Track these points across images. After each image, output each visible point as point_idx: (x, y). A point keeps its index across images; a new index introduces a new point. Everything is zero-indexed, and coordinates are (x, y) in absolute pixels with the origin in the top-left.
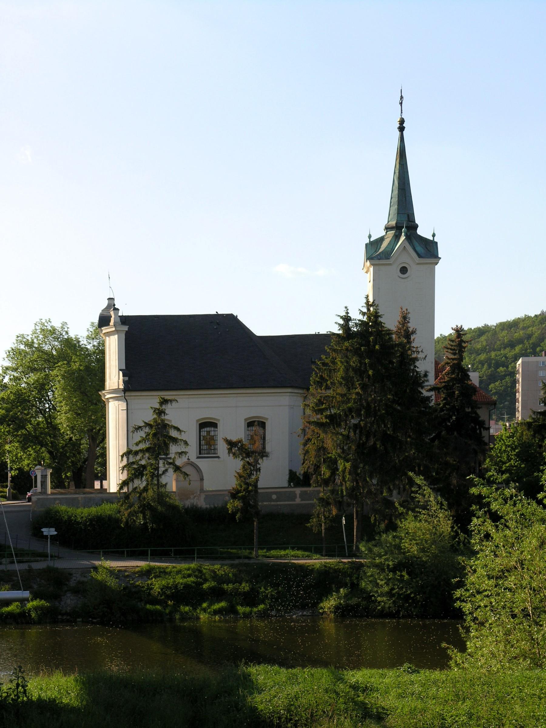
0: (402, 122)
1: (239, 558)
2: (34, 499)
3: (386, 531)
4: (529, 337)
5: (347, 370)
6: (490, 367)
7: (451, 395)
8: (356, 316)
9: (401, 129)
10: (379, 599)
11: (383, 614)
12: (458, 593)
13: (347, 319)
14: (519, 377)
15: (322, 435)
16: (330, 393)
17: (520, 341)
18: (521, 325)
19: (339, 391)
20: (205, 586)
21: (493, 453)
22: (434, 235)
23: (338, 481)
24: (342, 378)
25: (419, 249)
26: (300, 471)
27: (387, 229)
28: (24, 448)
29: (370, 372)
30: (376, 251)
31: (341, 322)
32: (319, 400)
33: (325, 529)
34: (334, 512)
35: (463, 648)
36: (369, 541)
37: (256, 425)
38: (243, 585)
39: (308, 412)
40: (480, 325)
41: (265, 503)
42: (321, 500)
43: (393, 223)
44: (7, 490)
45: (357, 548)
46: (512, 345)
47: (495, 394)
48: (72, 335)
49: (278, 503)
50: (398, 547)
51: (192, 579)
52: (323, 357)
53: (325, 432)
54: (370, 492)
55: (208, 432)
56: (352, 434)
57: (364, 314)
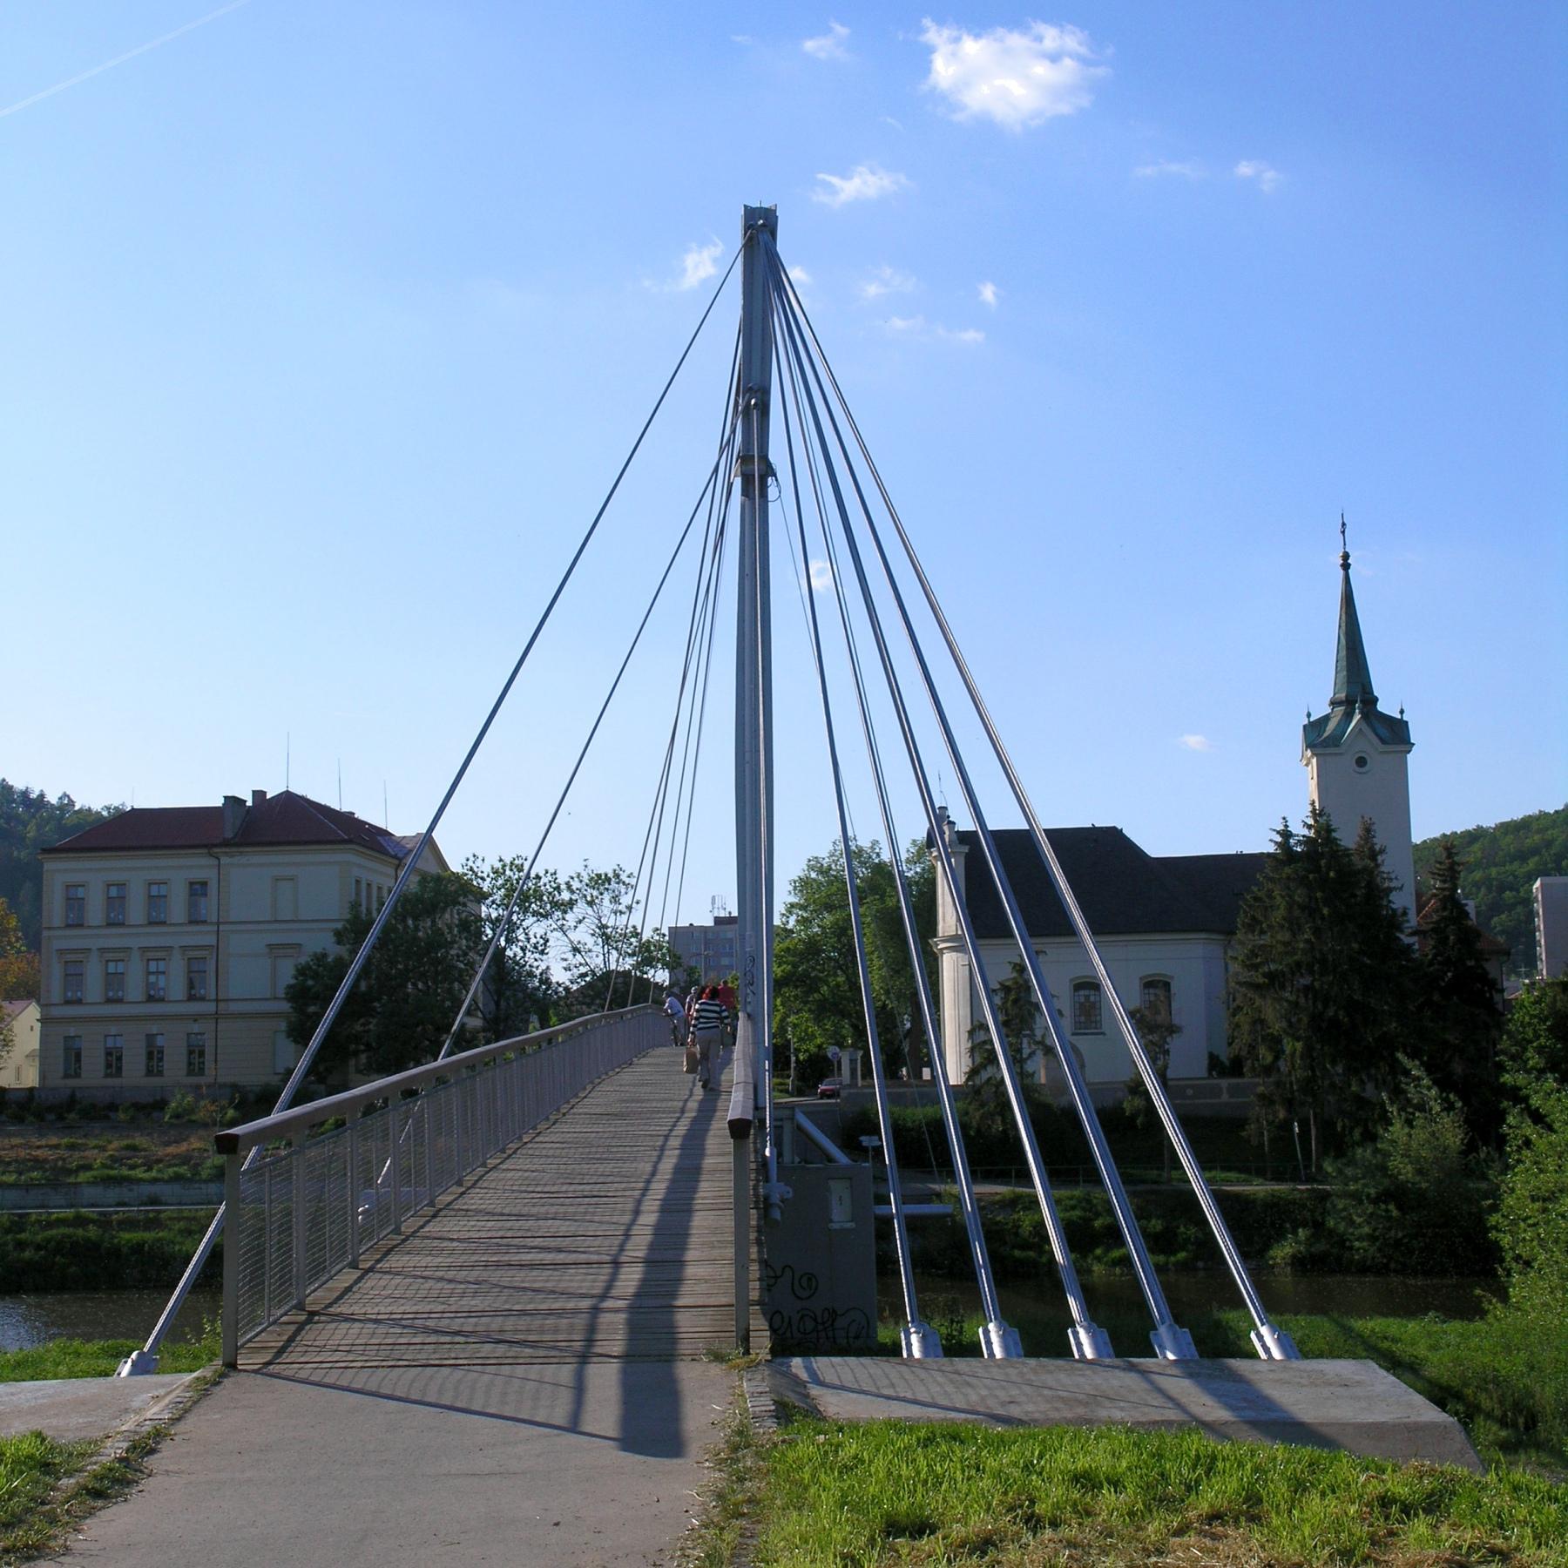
1: (1143, 1182)
2: (844, 1093)
3: (1361, 1144)
4: (1549, 844)
5: (1290, 908)
6: (1489, 890)
7: (1443, 941)
8: (1298, 830)
9: (1346, 566)
10: (1357, 1244)
11: (1363, 1269)
12: (1494, 1219)
13: (1286, 834)
14: (1538, 907)
15: (1258, 1002)
16: (1266, 939)
17: (1535, 851)
18: (1535, 826)
19: (1279, 937)
20: (1097, 1223)
21: (1511, 1026)
22: (1402, 712)
23: (1283, 1065)
24: (1284, 919)
25: (1383, 732)
26: (1225, 1055)
27: (1334, 703)
28: (818, 1020)
29: (1326, 911)
30: (1319, 736)
31: (1279, 839)
32: (1252, 951)
33: (1271, 1140)
34: (1282, 1115)
35: (1504, 1298)
36: (1337, 1157)
37: (1157, 986)
38: (1153, 1221)
39: (1235, 967)
40: (1471, 826)
42: (1262, 1097)
43: (1343, 696)
44: (790, 1081)
45: (1320, 1168)
46: (1522, 857)
47: (1502, 932)
50: (1383, 1168)
51: (1078, 1213)
52: (1255, 889)
53: (1263, 997)
54: (1333, 1085)
55: (1087, 997)
56: (1302, 1000)
57: (1309, 827)
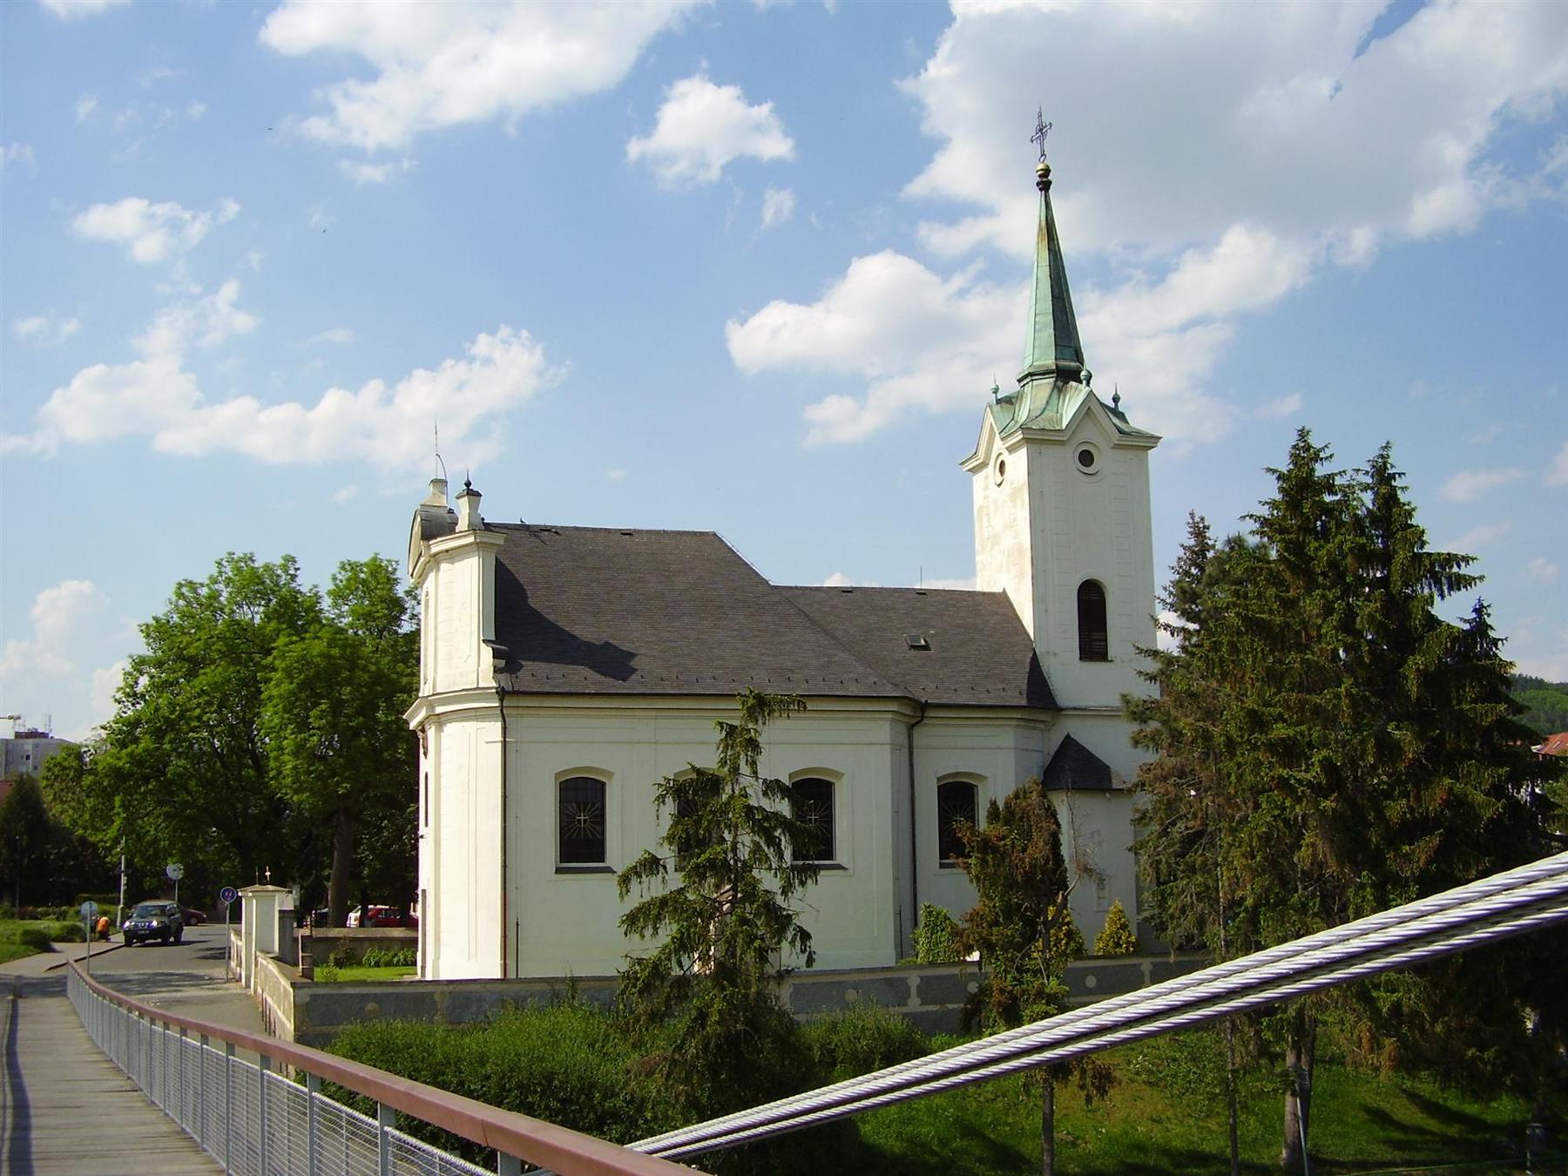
0: (1046, 172)
9: (1045, 185)
22: (1116, 399)
41: (950, 1006)
48: (304, 584)
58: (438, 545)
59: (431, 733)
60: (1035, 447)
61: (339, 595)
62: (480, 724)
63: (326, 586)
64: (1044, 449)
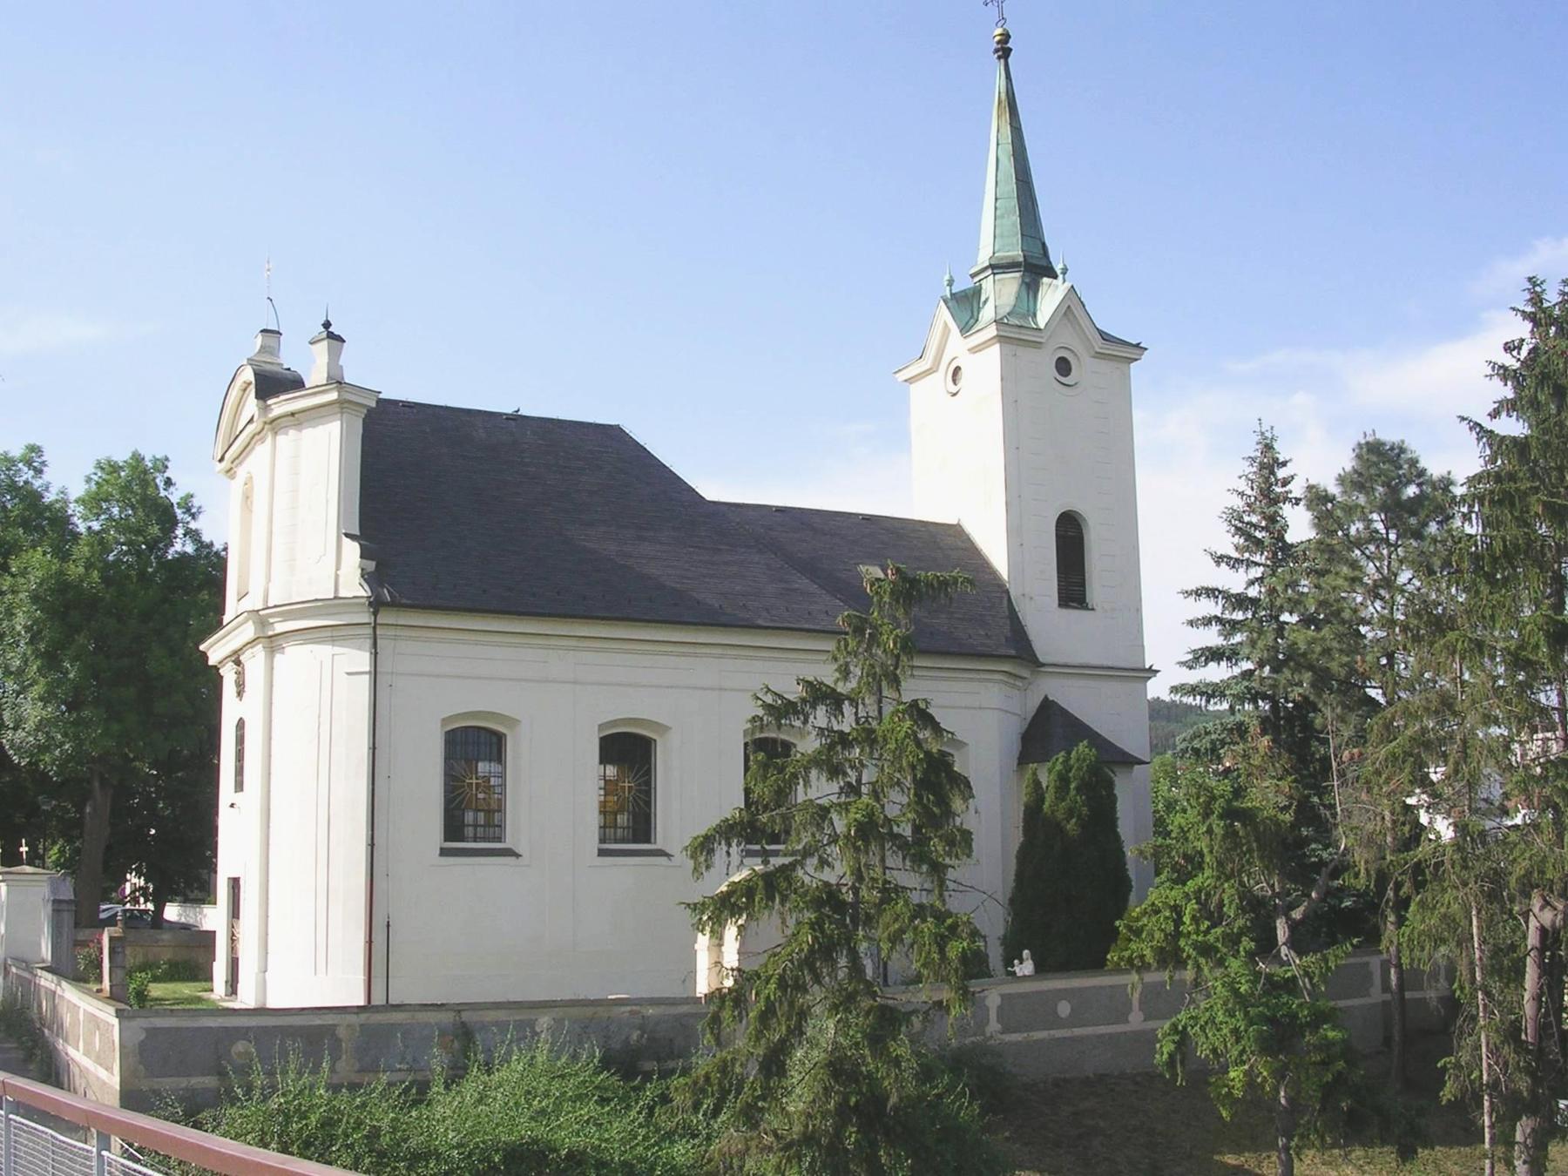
0: (1006, 37)
49: (1078, 1031)
58: (281, 405)
59: (255, 661)
60: (1009, 348)
61: (94, 502)
62: (337, 650)
63: (77, 489)
64: (1021, 351)
